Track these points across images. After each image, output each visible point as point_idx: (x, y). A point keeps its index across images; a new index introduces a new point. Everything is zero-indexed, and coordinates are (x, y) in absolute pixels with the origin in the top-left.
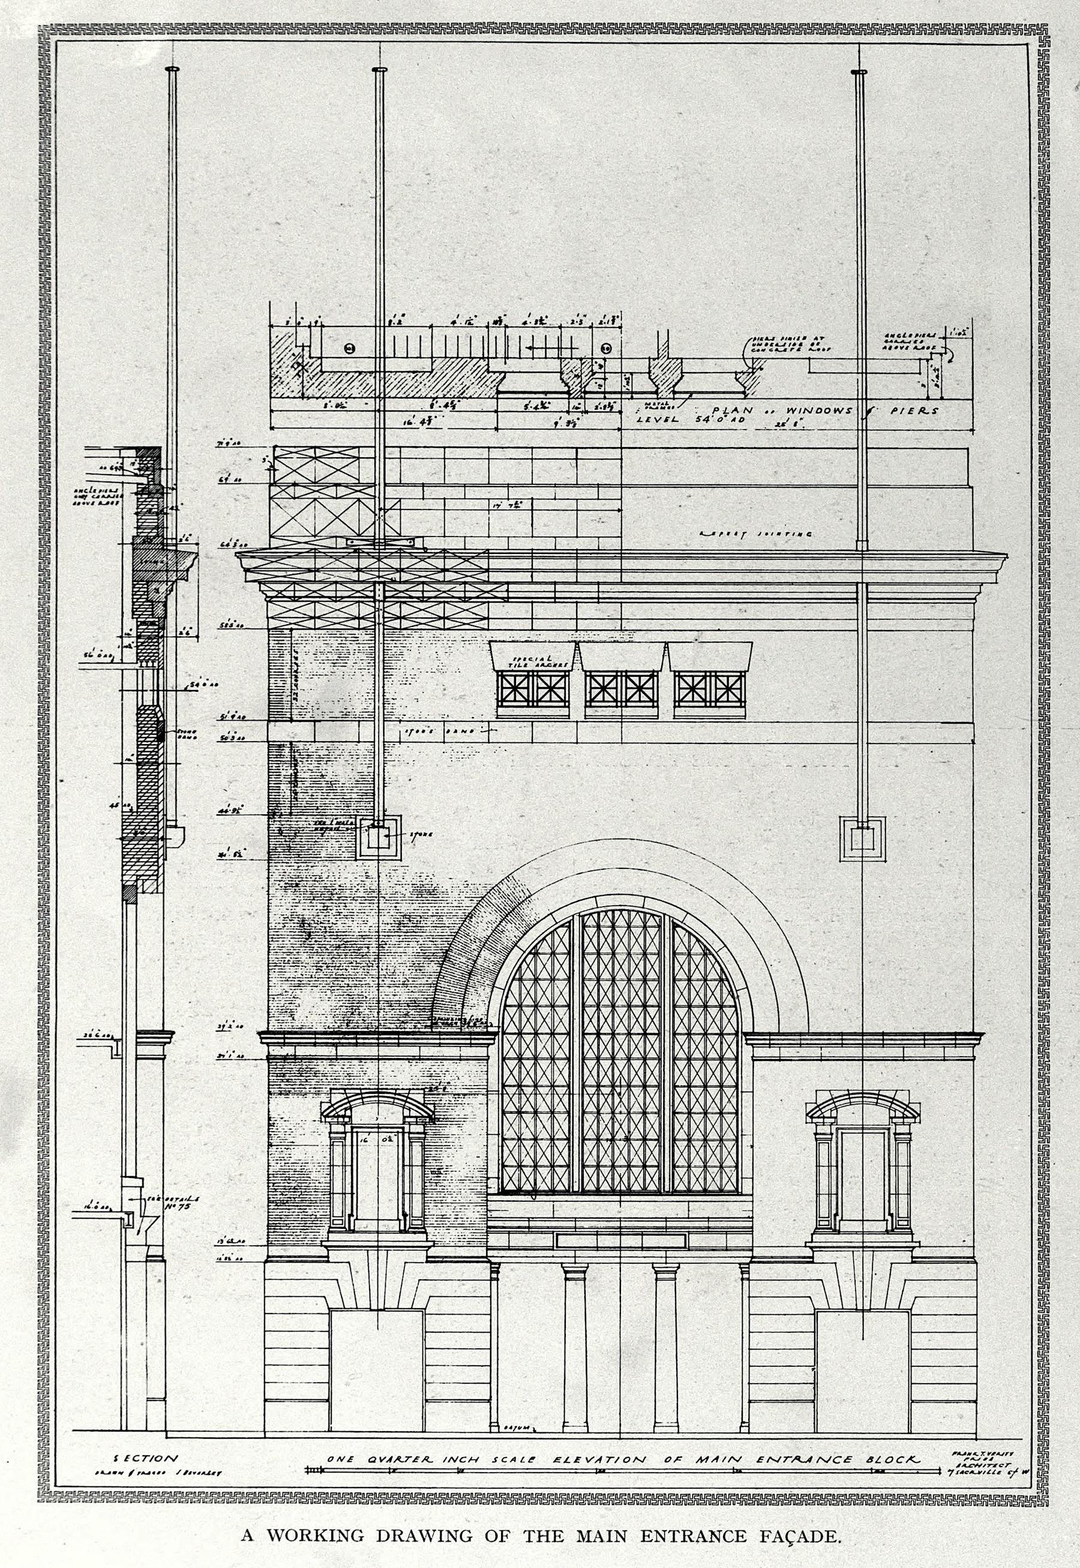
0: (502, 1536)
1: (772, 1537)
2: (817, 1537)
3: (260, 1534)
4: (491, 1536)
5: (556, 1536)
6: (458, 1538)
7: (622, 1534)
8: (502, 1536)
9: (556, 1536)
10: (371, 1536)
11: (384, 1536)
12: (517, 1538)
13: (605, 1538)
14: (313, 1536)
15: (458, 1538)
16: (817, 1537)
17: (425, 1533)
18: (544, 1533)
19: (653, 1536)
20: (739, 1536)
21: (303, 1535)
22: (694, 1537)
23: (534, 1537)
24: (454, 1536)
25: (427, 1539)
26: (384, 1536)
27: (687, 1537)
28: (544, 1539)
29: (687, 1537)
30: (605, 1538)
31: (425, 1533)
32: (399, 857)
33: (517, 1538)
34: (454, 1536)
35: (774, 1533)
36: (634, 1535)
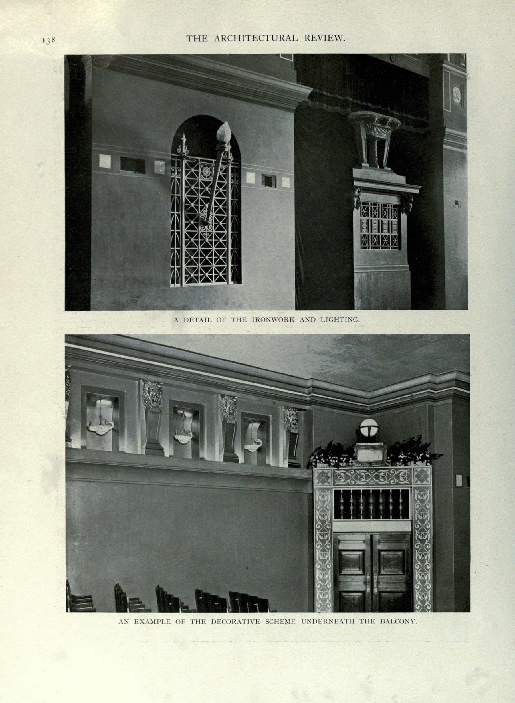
0: (223, 320)
1: (339, 621)
2: (315, 621)
3: (181, 320)
4: (178, 622)
8: (223, 320)
11: (214, 622)
13: (204, 320)
14: (289, 320)
16: (315, 621)
17: (337, 37)
22: (285, 39)
23: (235, 320)
24: (288, 622)
25: (339, 39)
26: (214, 622)
29: (282, 38)
30: (204, 320)
31: (337, 37)
33: (300, 37)
34: (288, 622)
36: (211, 39)
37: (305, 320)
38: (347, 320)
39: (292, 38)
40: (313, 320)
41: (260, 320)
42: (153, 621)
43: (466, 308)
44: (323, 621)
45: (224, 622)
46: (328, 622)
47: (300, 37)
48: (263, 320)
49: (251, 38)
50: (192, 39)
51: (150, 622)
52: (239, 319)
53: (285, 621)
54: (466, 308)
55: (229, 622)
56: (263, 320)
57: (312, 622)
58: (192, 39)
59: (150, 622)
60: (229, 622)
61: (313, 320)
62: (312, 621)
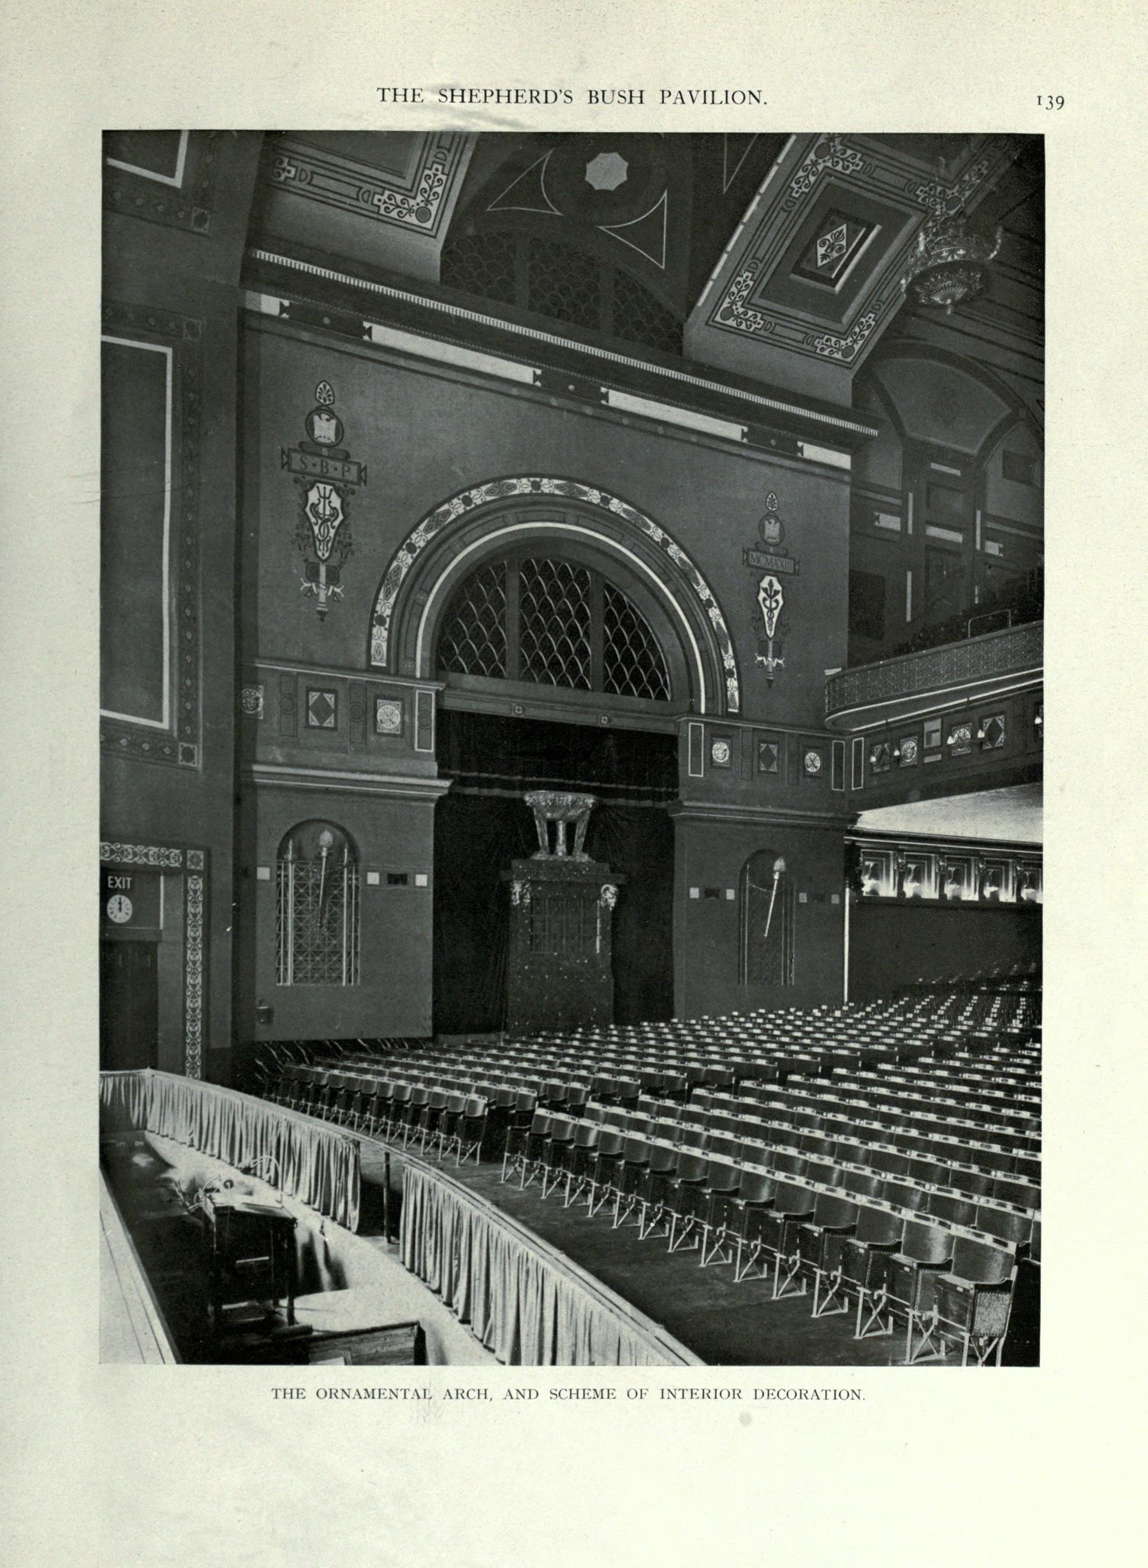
5: (299, 1393)
6: (747, 94)
7: (757, 95)
8: (641, 1394)
9: (299, 1393)
10: (620, 1394)
11: (759, 1394)
12: (653, 1395)
15: (747, 94)
18: (288, 1391)
19: (388, 1394)
20: (593, 97)
21: (370, 1394)
24: (599, 1394)
26: (759, 1394)
27: (837, 1395)
28: (288, 1396)
29: (837, 1395)
32: (710, 323)
33: (653, 1395)
34: (599, 1394)
35: (674, 94)
37: (514, 1394)
38: (665, 1396)
39: (668, 1393)
40: (534, 1394)
41: (465, 1395)
42: (370, 1391)
43: (107, 134)
44: (700, 1393)
45: (783, 1394)
46: (339, 1395)
47: (747, 1394)
48: (844, 1395)
49: (687, 1394)
50: (389, 95)
51: (363, 1394)
52: (288, 1391)
53: (592, 1394)
54: (107, 134)
55: (792, 1394)
56: (844, 1395)
57: (527, 1396)
58: (389, 95)
59: (363, 1394)
60: (792, 1394)
61: (534, 1394)
62: (527, 1393)
